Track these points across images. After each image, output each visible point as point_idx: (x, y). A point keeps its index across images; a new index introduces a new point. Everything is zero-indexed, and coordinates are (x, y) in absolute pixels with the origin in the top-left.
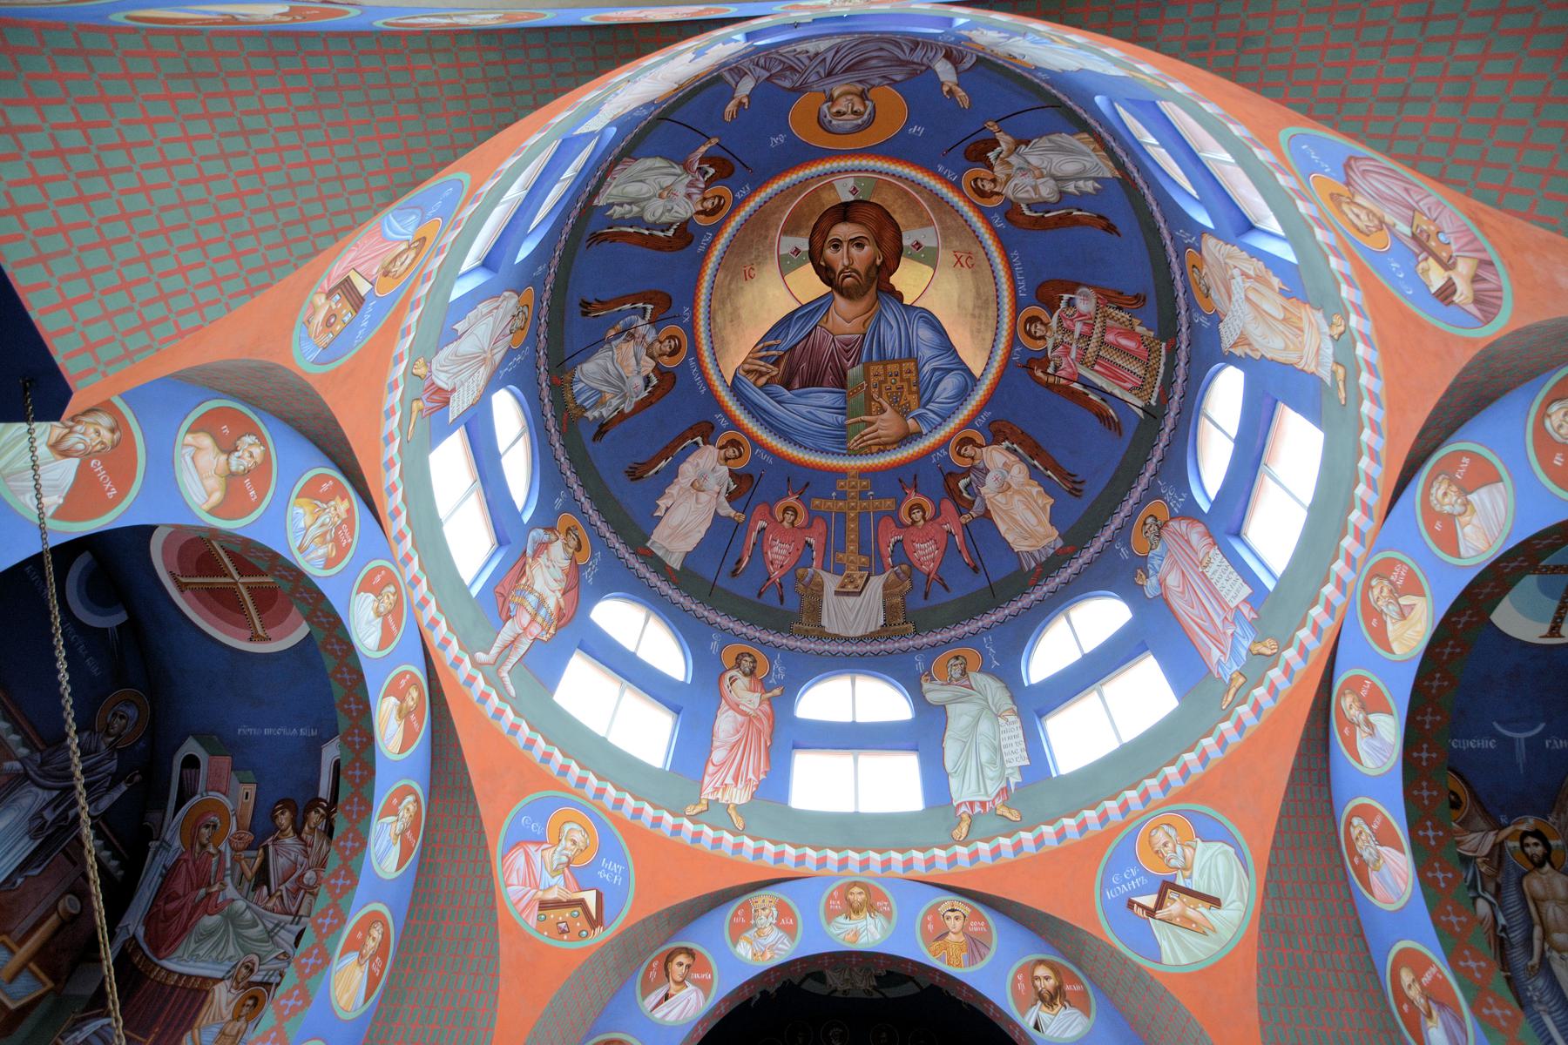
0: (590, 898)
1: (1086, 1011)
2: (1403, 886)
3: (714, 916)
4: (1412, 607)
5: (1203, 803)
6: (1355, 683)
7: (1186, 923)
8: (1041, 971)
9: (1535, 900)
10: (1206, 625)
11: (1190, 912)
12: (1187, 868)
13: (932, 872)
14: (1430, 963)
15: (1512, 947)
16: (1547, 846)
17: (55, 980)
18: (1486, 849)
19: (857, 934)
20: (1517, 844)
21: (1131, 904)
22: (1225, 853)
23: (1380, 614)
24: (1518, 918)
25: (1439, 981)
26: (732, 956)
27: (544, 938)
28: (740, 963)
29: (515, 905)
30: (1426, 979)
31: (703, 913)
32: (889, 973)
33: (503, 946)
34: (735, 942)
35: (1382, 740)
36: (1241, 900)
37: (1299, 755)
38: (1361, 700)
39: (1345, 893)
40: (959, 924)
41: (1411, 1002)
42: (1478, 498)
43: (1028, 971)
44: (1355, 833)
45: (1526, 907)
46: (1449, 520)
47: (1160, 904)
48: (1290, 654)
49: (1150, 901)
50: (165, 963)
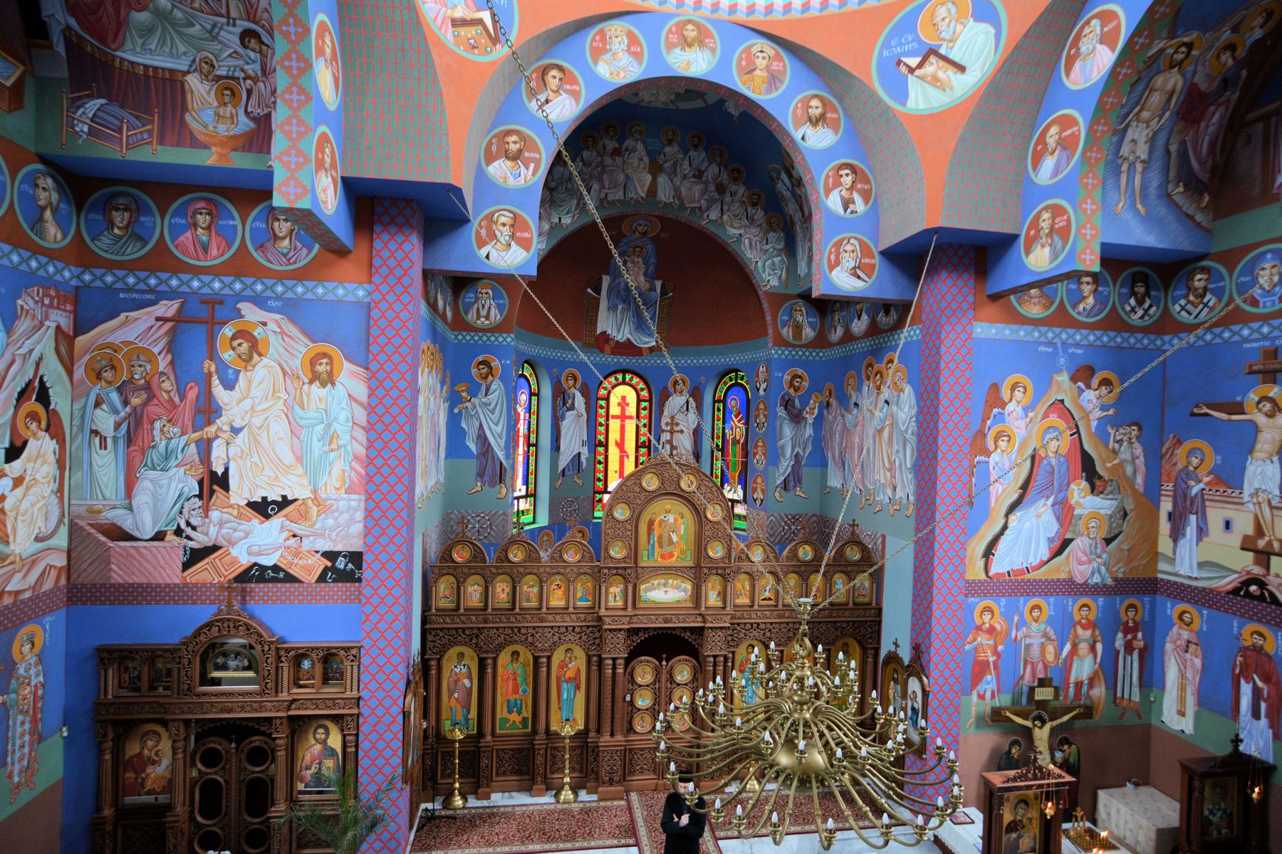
0: (486, 16)
1: (836, 132)
2: (1095, 74)
3: (577, 38)
7: (935, 81)
8: (815, 103)
11: (941, 74)
13: (752, 18)
17: (24, 64)
19: (688, 64)
21: (899, 62)
25: (1075, 137)
26: (592, 72)
27: (461, 51)
28: (598, 80)
29: (435, 20)
31: (568, 35)
32: (687, 91)
33: (435, 56)
34: (596, 63)
40: (765, 62)
43: (806, 103)
44: (1087, 30)
47: (920, 66)
49: (913, 62)
50: (118, 53)
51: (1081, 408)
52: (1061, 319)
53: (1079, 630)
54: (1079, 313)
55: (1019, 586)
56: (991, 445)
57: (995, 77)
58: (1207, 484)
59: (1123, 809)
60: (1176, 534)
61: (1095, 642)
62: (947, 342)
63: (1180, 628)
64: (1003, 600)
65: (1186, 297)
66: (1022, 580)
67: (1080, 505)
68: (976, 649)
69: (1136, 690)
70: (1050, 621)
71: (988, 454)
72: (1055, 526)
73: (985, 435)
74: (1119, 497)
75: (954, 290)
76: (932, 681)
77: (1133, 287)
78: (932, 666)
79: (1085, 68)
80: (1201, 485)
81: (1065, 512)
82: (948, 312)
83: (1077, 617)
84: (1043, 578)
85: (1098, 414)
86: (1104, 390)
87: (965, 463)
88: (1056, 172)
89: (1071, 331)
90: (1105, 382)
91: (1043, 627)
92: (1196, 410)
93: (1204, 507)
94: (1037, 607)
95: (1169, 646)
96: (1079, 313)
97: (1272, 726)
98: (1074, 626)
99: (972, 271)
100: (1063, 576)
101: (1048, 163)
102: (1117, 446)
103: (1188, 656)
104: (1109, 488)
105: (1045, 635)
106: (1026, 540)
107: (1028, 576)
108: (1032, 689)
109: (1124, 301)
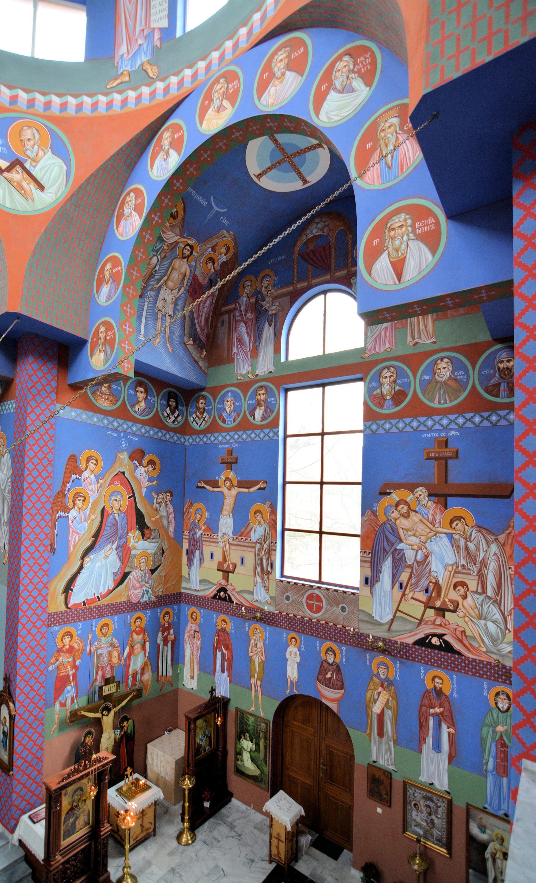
4: (225, 108)
5: (66, 132)
6: (177, 128)
7: (19, 188)
9: (173, 268)
10: (130, 23)
11: (24, 184)
12: (35, 161)
14: (120, 265)
15: (154, 278)
16: (191, 253)
18: (171, 241)
20: (183, 246)
22: (61, 167)
23: (211, 100)
24: (163, 271)
25: (119, 273)
30: (115, 270)
35: (167, 165)
36: (56, 195)
37: (129, 144)
38: (173, 139)
39: (106, 223)
41: (104, 275)
42: (290, 76)
44: (128, 199)
45: (168, 268)
46: (272, 76)
48: (160, 85)
51: (135, 478)
52: (122, 413)
53: (135, 636)
54: (135, 412)
55: (92, 610)
56: (70, 503)
57: (66, 203)
58: (204, 531)
59: (160, 753)
60: (190, 564)
61: (145, 642)
62: (33, 416)
63: (191, 623)
64: (80, 624)
65: (196, 413)
66: (95, 607)
67: (135, 547)
68: (58, 668)
69: (170, 668)
70: (114, 635)
71: (68, 510)
72: (118, 564)
73: (65, 495)
74: (159, 540)
75: (40, 374)
76: (17, 704)
77: (168, 401)
78: (18, 692)
79: (126, 224)
80: (201, 532)
81: (124, 553)
82: (34, 391)
83: (133, 627)
84: (110, 603)
85: (147, 484)
86: (150, 468)
87: (48, 518)
88: (109, 298)
89: (130, 424)
90: (151, 462)
91: (110, 638)
92: (199, 485)
93: (202, 545)
94: (106, 625)
95: (186, 635)
96: (135, 412)
97: (229, 676)
98: (131, 634)
99: (56, 362)
100: (124, 599)
101: (105, 290)
102: (158, 506)
103: (195, 640)
104: (153, 535)
105: (112, 645)
106: (97, 577)
107: (98, 603)
108: (101, 688)
109: (163, 410)
